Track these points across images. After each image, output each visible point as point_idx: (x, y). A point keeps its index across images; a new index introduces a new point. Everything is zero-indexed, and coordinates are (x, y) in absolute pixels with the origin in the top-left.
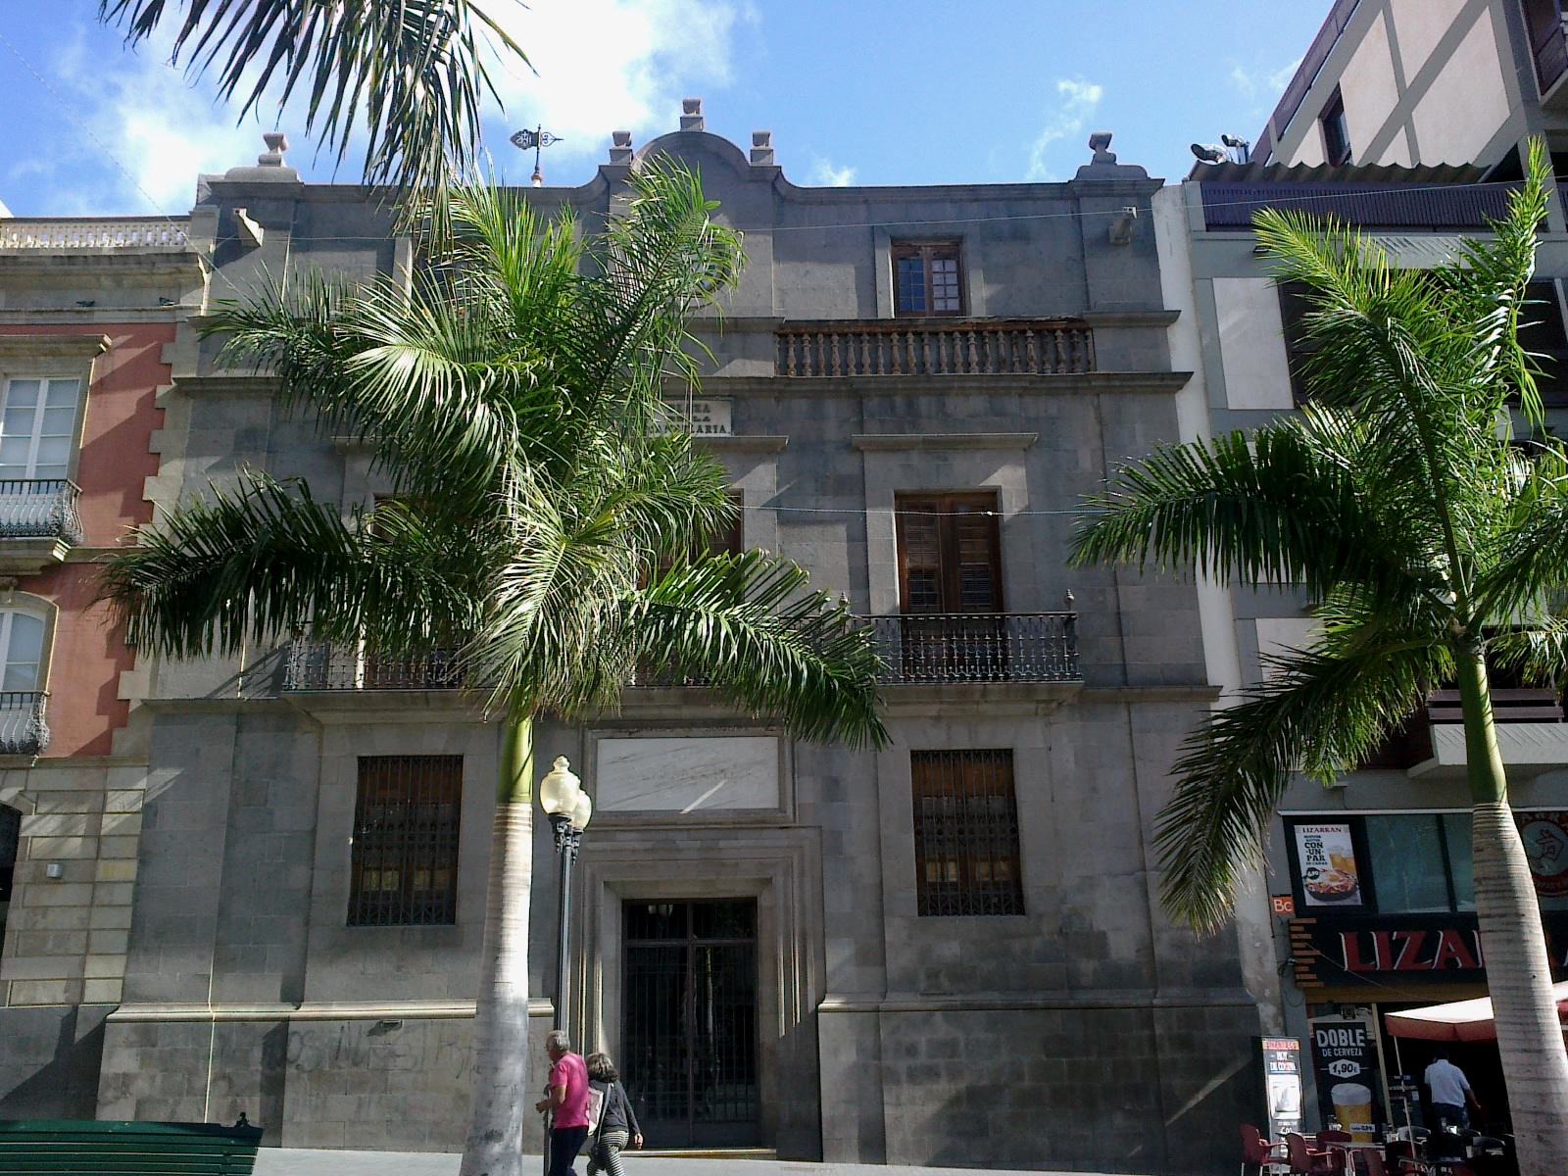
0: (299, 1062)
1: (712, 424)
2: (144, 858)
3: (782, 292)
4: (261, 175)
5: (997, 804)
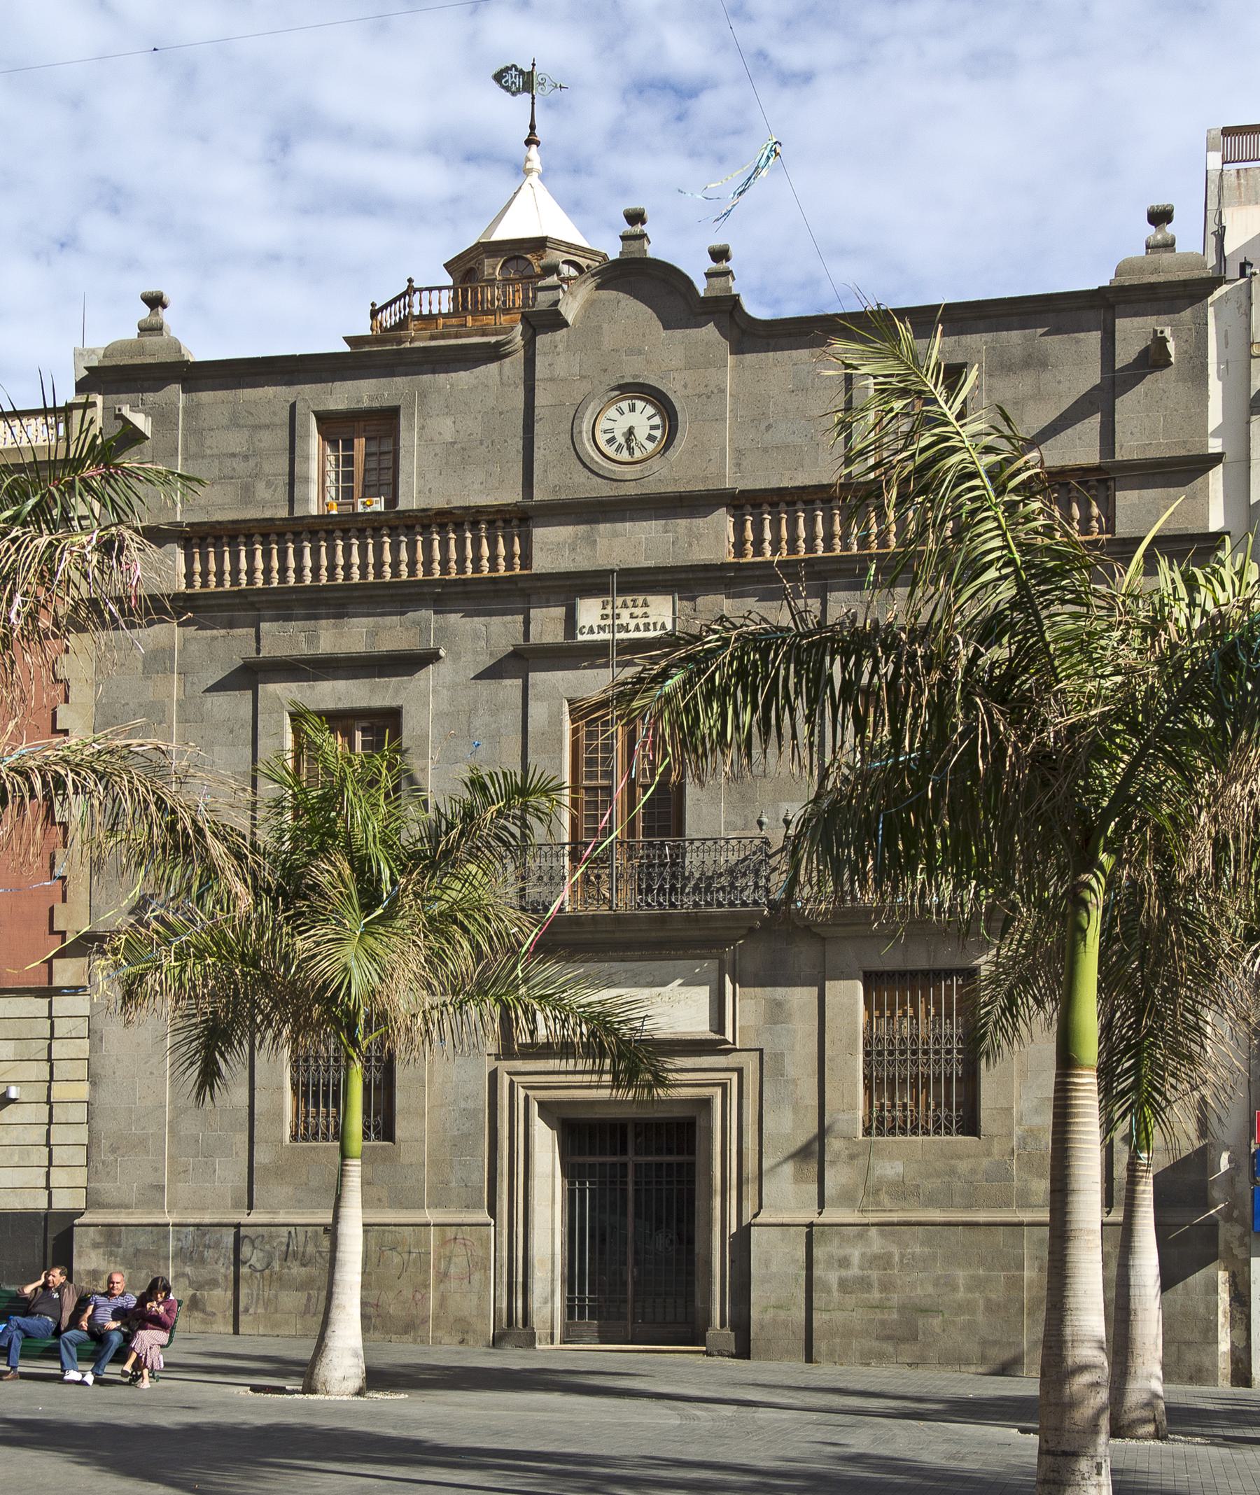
0: (251, 1262)
1: (651, 620)
2: (93, 1079)
3: (739, 453)
4: (141, 350)
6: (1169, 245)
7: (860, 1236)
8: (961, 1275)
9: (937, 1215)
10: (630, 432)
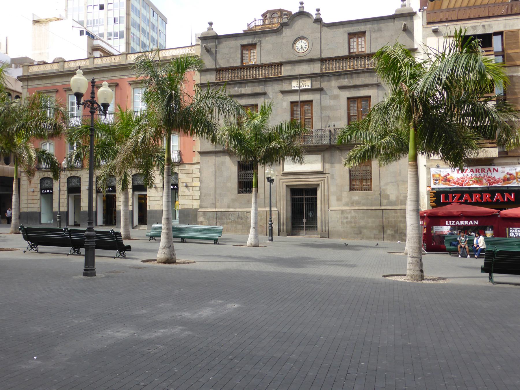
2: (201, 182)
5: (354, 183)
6: (405, 6)
7: (350, 212)
8: (370, 220)
9: (365, 208)
10: (302, 47)
